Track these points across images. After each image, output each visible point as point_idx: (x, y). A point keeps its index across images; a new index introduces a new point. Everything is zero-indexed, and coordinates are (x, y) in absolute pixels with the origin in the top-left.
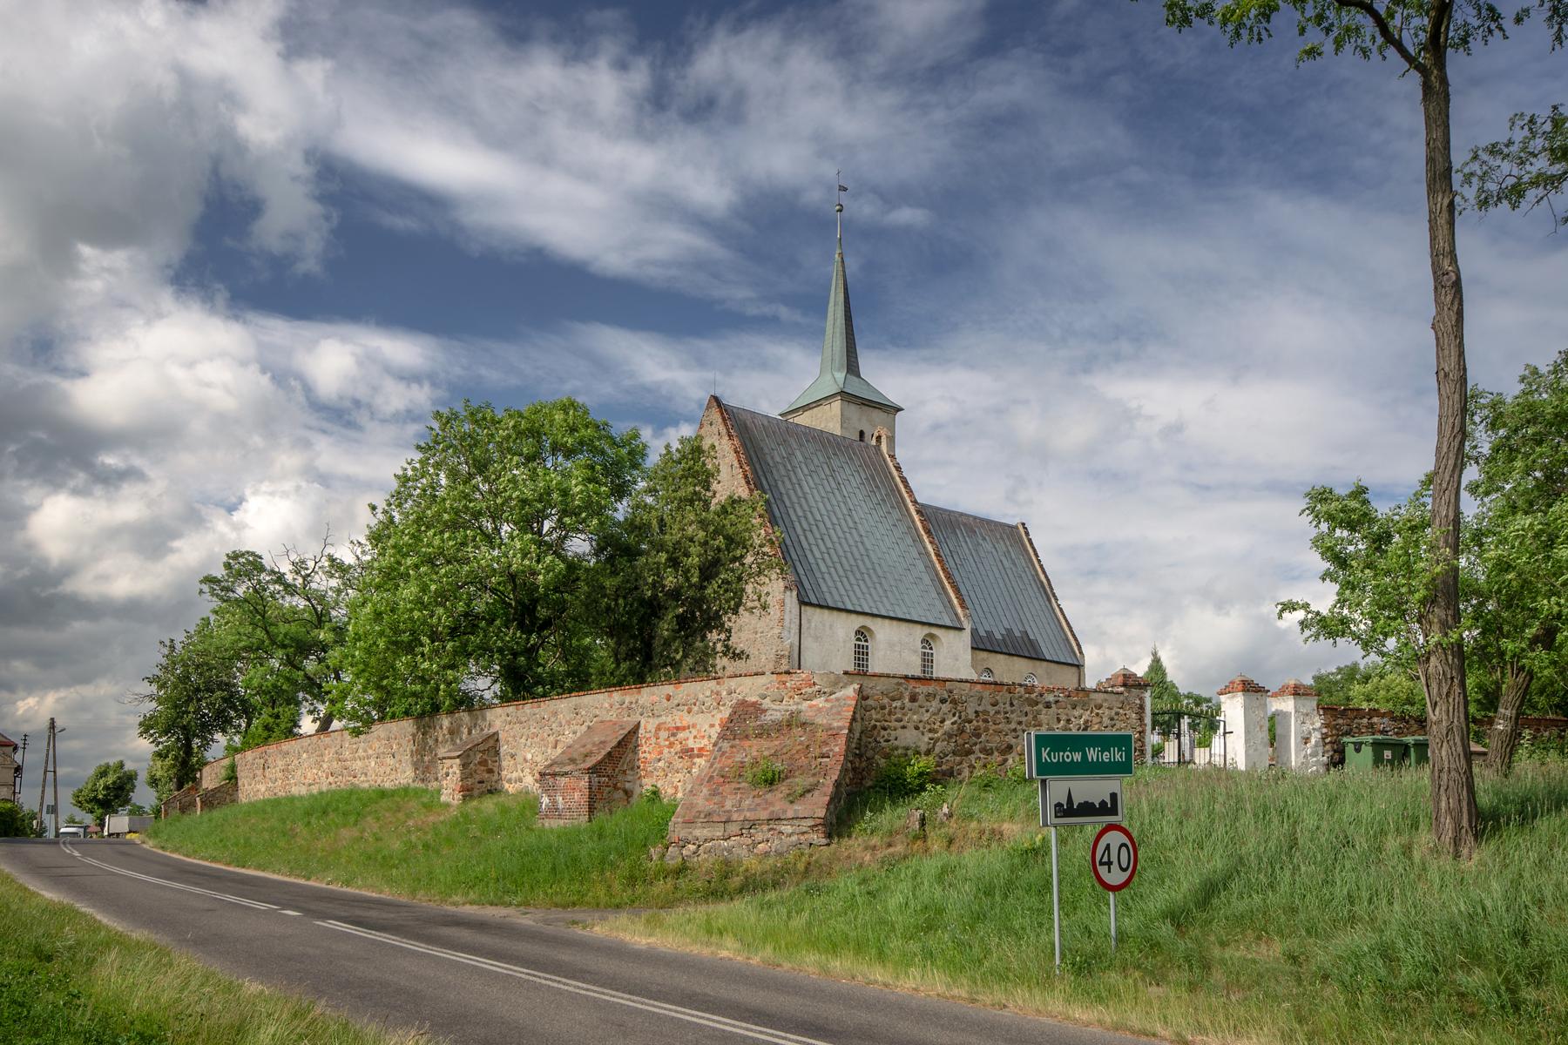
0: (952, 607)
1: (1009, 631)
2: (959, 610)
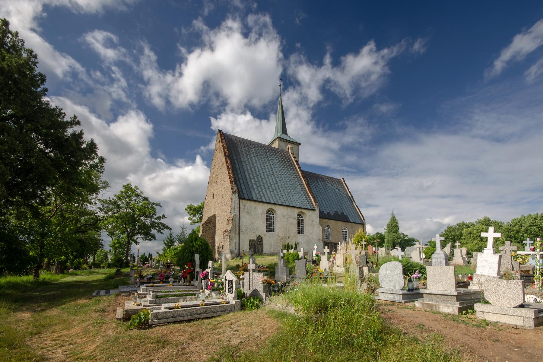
0: (311, 202)
2: (314, 203)
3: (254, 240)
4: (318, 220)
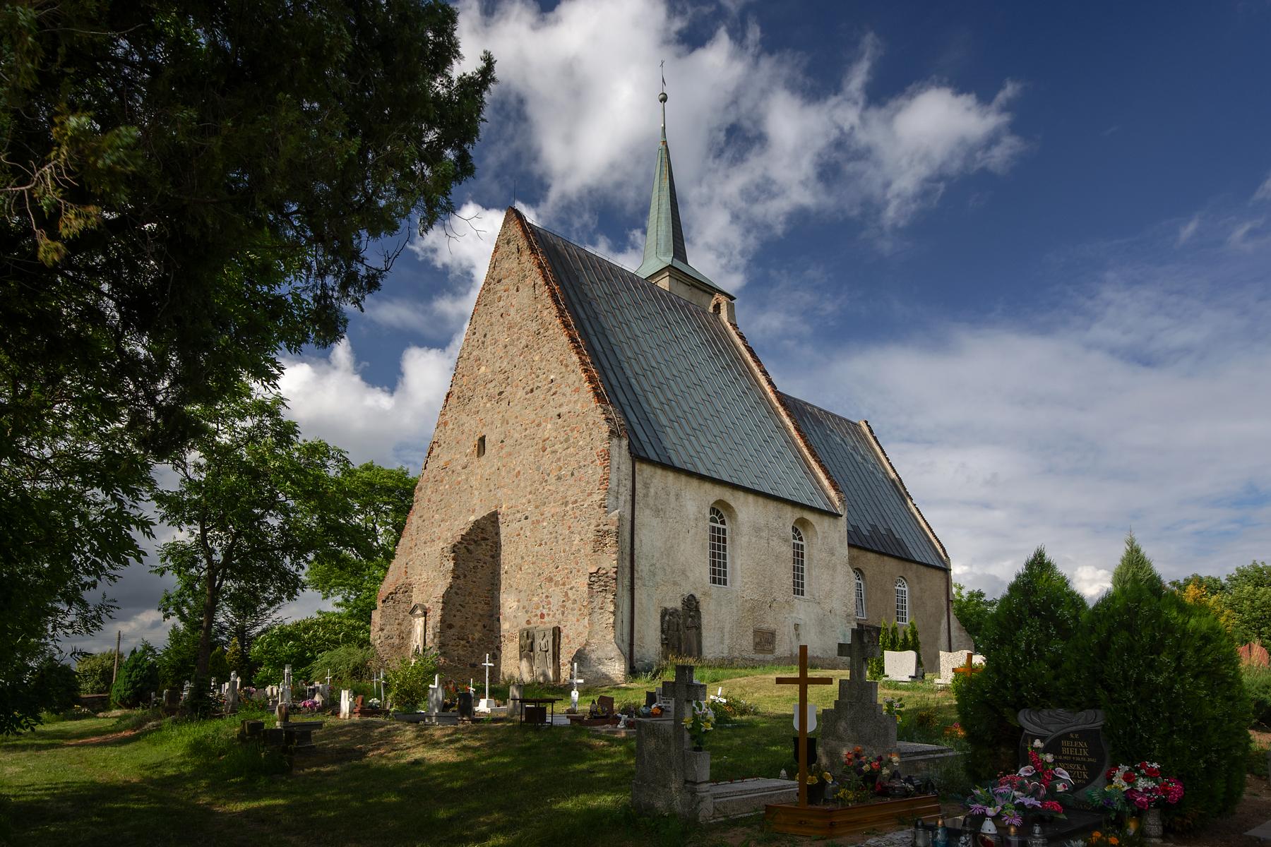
1: (874, 527)
2: (832, 493)
3: (674, 613)
4: (843, 551)
